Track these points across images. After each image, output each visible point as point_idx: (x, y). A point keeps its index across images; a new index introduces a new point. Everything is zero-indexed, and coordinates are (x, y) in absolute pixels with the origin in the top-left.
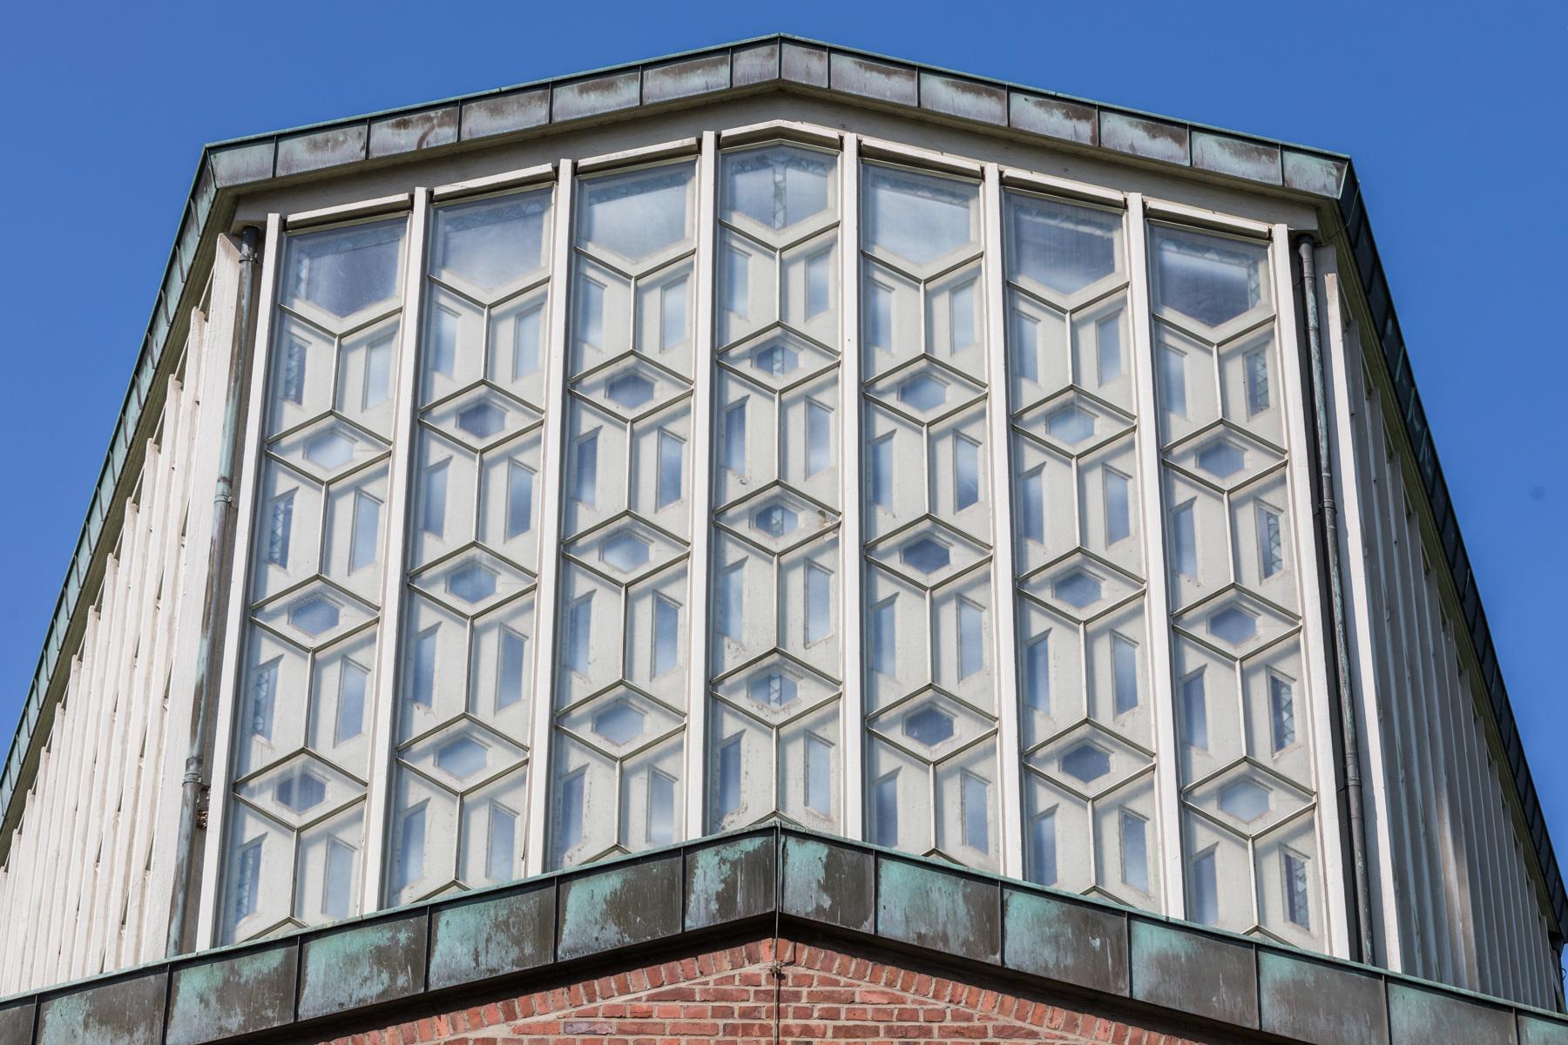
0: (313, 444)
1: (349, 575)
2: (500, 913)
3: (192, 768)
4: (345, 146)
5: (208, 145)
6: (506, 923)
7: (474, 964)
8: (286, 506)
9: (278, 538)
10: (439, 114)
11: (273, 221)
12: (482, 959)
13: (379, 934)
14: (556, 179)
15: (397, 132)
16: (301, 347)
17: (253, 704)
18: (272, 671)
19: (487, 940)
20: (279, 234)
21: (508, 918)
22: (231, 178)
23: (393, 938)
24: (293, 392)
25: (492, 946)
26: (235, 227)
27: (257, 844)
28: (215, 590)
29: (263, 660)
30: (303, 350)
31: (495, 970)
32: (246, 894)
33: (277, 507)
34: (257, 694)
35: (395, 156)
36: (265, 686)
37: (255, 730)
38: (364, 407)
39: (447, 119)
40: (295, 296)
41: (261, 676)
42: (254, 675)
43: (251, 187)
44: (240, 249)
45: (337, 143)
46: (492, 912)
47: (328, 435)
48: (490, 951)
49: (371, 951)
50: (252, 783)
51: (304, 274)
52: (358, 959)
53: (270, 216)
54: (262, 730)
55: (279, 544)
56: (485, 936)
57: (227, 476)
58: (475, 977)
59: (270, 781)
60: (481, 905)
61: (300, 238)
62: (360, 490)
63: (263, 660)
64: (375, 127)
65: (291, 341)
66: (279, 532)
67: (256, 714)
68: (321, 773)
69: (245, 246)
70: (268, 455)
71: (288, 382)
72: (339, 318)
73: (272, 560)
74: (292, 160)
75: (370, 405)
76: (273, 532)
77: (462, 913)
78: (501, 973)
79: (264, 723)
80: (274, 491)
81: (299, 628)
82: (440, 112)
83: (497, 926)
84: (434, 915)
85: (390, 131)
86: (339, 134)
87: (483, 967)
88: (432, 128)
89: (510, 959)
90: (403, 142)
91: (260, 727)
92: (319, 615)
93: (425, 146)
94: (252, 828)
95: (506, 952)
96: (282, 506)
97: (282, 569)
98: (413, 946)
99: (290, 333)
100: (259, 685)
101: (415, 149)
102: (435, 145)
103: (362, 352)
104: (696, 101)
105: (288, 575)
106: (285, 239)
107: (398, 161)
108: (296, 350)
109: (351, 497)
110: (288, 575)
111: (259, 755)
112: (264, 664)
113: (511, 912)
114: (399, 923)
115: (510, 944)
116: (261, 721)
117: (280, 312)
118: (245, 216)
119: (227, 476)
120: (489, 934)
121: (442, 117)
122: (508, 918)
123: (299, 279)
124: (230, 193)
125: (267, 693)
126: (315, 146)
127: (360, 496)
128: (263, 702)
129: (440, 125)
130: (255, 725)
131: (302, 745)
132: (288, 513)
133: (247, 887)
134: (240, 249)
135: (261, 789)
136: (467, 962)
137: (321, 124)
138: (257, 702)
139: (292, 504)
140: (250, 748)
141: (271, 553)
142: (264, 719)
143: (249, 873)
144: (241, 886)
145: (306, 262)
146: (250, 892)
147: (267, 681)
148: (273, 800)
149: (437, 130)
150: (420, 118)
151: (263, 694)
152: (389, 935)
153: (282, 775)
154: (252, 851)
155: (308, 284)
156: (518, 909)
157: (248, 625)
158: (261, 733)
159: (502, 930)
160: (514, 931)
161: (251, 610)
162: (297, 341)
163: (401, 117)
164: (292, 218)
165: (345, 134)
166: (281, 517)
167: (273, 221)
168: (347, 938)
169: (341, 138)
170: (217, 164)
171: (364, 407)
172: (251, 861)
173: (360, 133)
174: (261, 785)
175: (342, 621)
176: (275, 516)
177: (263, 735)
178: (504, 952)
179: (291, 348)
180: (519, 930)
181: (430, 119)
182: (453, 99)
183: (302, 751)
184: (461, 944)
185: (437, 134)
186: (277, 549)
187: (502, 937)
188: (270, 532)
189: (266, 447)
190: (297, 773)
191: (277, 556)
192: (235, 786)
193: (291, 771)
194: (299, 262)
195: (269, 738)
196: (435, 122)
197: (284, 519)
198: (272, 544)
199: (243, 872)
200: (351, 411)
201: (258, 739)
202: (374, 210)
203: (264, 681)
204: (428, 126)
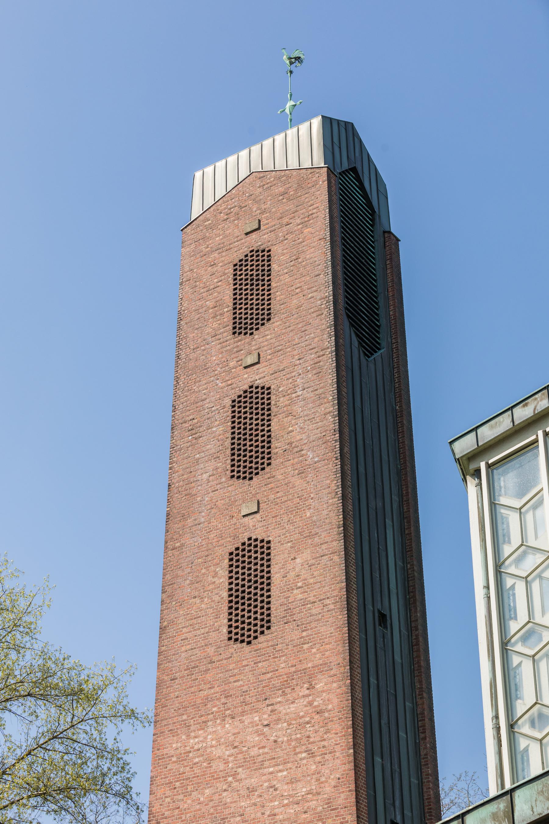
0: (519, 560)
1: (543, 617)
2: (539, 787)
3: (494, 721)
4: (504, 423)
5: (449, 441)
6: (542, 791)
7: (532, 813)
8: (512, 592)
9: (512, 607)
10: (540, 396)
11: (483, 465)
12: (535, 810)
13: (492, 807)
14: (537, 441)
15: (524, 409)
16: (506, 518)
17: (514, 686)
18: (520, 669)
19: (536, 801)
20: (544, 438)
21: (543, 788)
22: (461, 453)
23: (498, 807)
24: (507, 539)
25: (538, 803)
26: (472, 472)
27: (526, 749)
28: (489, 638)
29: (515, 665)
30: (507, 518)
31: (541, 814)
32: (526, 773)
33: (509, 594)
34: (515, 681)
35: (527, 420)
36: (518, 677)
37: (517, 698)
38: (536, 537)
39: (543, 397)
40: (500, 495)
41: (515, 672)
42: (512, 673)
43: (472, 453)
44: (475, 480)
45: (500, 423)
46: (536, 787)
47: (524, 554)
48: (538, 805)
49: (490, 815)
50: (520, 722)
51: (502, 484)
52: (485, 820)
53: (481, 463)
54: (520, 697)
55: (513, 610)
56: (534, 799)
57: (486, 585)
58: (533, 819)
59: (525, 721)
60: (531, 785)
61: (495, 469)
62: (541, 576)
63: (515, 665)
64: (514, 410)
65: (502, 516)
66: (512, 605)
67: (516, 690)
68: (547, 711)
69: (476, 479)
70: (500, 572)
71: (504, 536)
72: (519, 500)
73: (511, 618)
74: (484, 436)
75: (539, 536)
76: (509, 605)
77: (524, 791)
78: (543, 815)
79: (520, 694)
80: (506, 587)
81: (527, 647)
82: (540, 394)
83: (538, 793)
84: (513, 794)
85: (521, 410)
86: (500, 418)
87: (536, 813)
88: (538, 403)
89: (546, 807)
90: (527, 413)
91: (519, 696)
92: (533, 639)
93: (536, 412)
94: (523, 743)
95: (544, 805)
96: (511, 592)
97: (515, 621)
98: (506, 810)
99: (500, 512)
100: (515, 677)
101: (532, 414)
102: (540, 410)
103: (531, 513)
104: (508, 433)
105: (518, 623)
106: (490, 472)
107: (529, 421)
108: (505, 519)
109: (537, 581)
110: (518, 623)
111: (520, 708)
112: (516, 666)
113: (544, 786)
114: (499, 800)
115: (545, 800)
116: (519, 693)
117: (493, 505)
118: (472, 466)
119: (486, 585)
120: (536, 798)
121: (541, 396)
122: (543, 788)
123: (500, 487)
124: (464, 458)
125: (519, 680)
126: (492, 427)
127: (542, 579)
128: (518, 684)
129: (541, 400)
130: (517, 695)
131: (535, 701)
132: (514, 595)
133: (526, 770)
134: (475, 480)
135: (523, 725)
136: (529, 812)
137: (495, 415)
138: (516, 685)
139: (515, 590)
140: (516, 705)
141: (510, 615)
142: (520, 692)
143: (525, 764)
144: (523, 770)
145: (502, 479)
146: (527, 772)
147: (518, 674)
148: (529, 728)
149: (540, 403)
150: (532, 400)
151: (518, 680)
152: (496, 806)
153: (530, 717)
154: (525, 754)
155: (505, 488)
156: (546, 783)
157: (505, 651)
158: (519, 698)
159: (541, 795)
160: (546, 794)
161: (504, 645)
162: (504, 515)
163: (523, 402)
164: (490, 462)
165: (503, 417)
166: (511, 598)
167: (483, 465)
168: (480, 811)
169: (502, 420)
170: (455, 448)
171: (536, 537)
172: (525, 758)
173: (509, 415)
174: (522, 723)
175: (544, 639)
176: (509, 598)
177: (520, 699)
178: (543, 805)
179: (503, 519)
180: (548, 793)
181: (536, 399)
182: (543, 387)
183: (536, 703)
184: (525, 805)
185: (540, 405)
186: (512, 613)
187: (541, 798)
188: (508, 605)
189: (498, 568)
190: (536, 715)
191: (513, 616)
192: (511, 726)
193: (533, 714)
194: (499, 479)
195: (523, 700)
196: (539, 399)
197: (513, 598)
198: (510, 611)
199: (523, 763)
200: (531, 542)
201: (519, 701)
202: (523, 447)
203: (517, 674)
204: (536, 402)
